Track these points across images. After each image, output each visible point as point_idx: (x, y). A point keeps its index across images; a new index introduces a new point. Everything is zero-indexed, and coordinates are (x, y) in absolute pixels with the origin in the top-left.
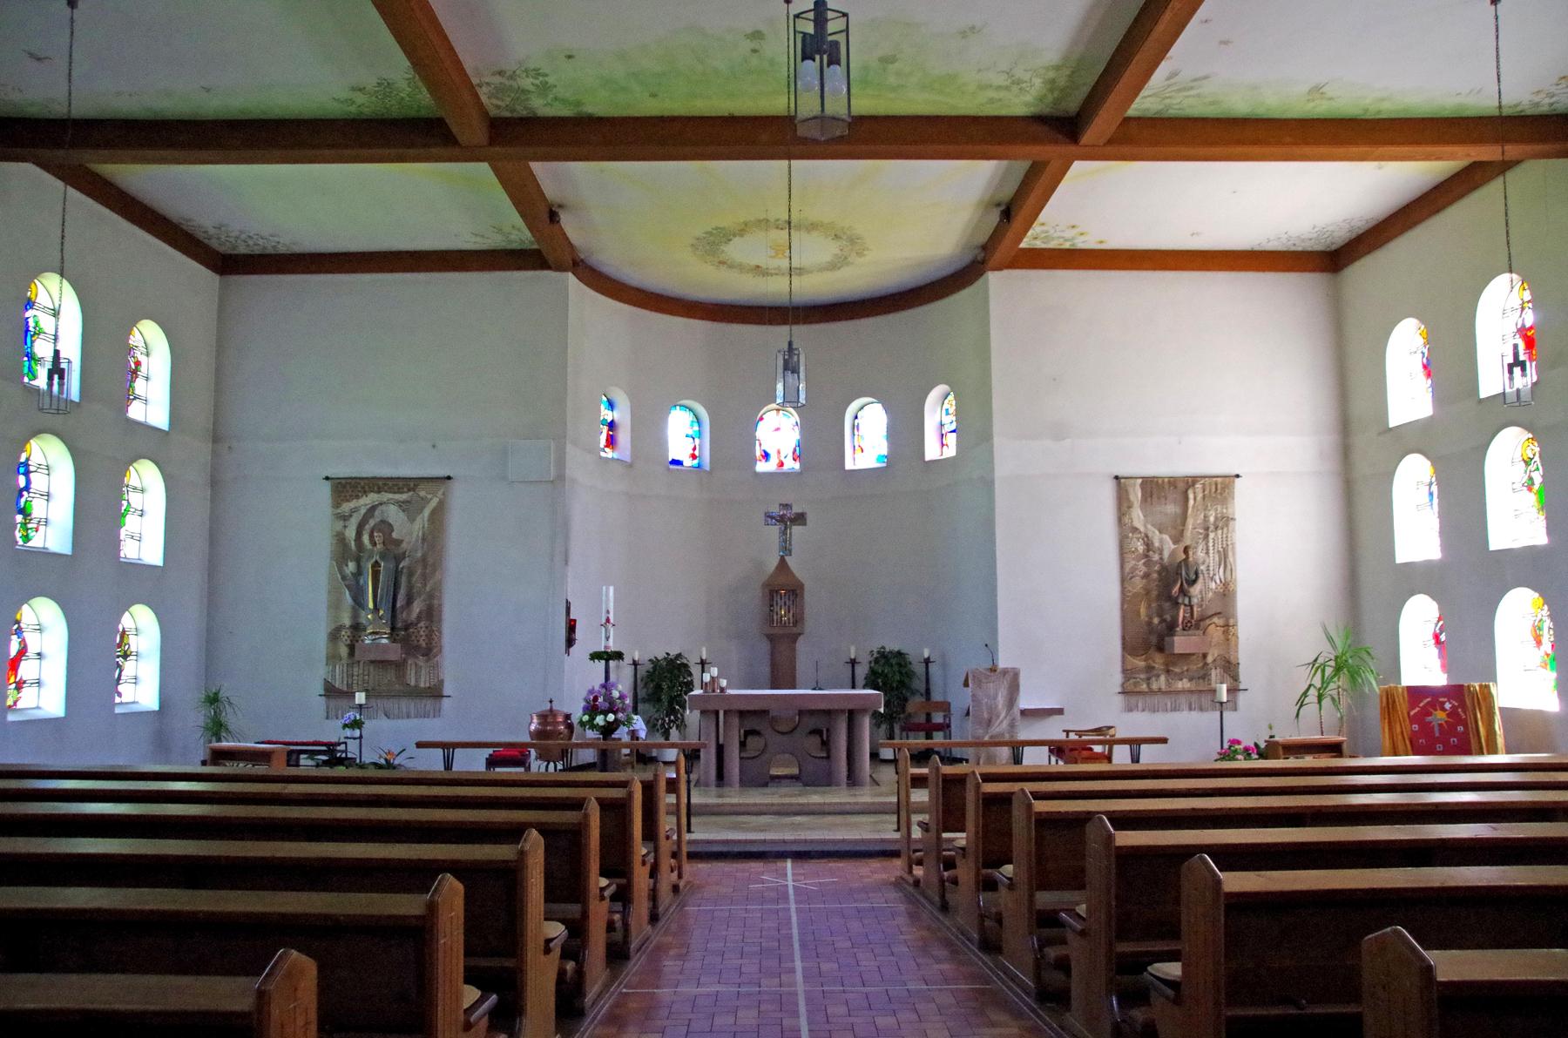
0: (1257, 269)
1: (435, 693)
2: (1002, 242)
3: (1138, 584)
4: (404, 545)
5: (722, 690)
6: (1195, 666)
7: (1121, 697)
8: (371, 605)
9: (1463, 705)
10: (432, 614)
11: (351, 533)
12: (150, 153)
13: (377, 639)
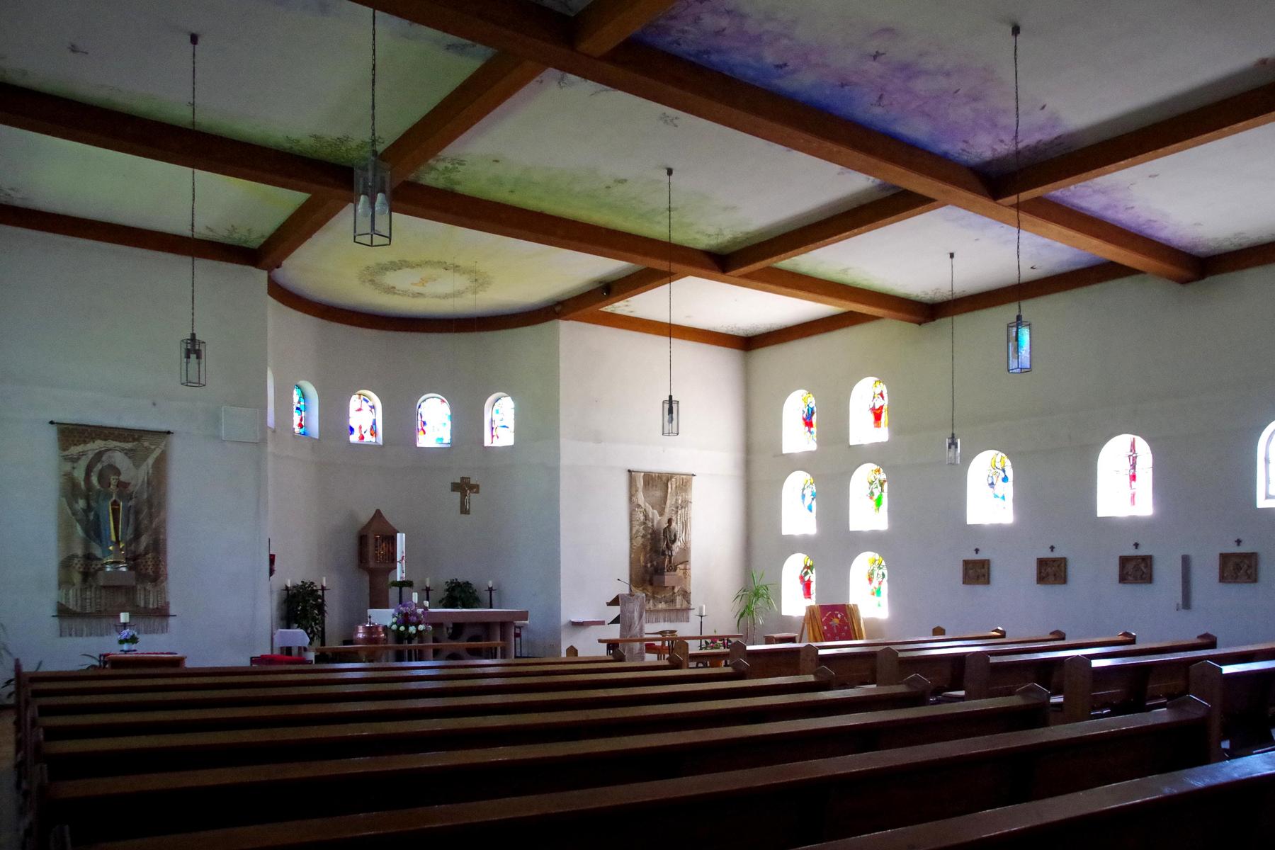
0: (707, 342)
1: (162, 613)
2: (585, 304)
3: (640, 541)
4: (131, 488)
5: (426, 609)
6: (669, 594)
7: (56, 620)
8: (114, 538)
9: (846, 615)
10: (158, 547)
11: (79, 474)
12: (783, 289)
13: (114, 566)
